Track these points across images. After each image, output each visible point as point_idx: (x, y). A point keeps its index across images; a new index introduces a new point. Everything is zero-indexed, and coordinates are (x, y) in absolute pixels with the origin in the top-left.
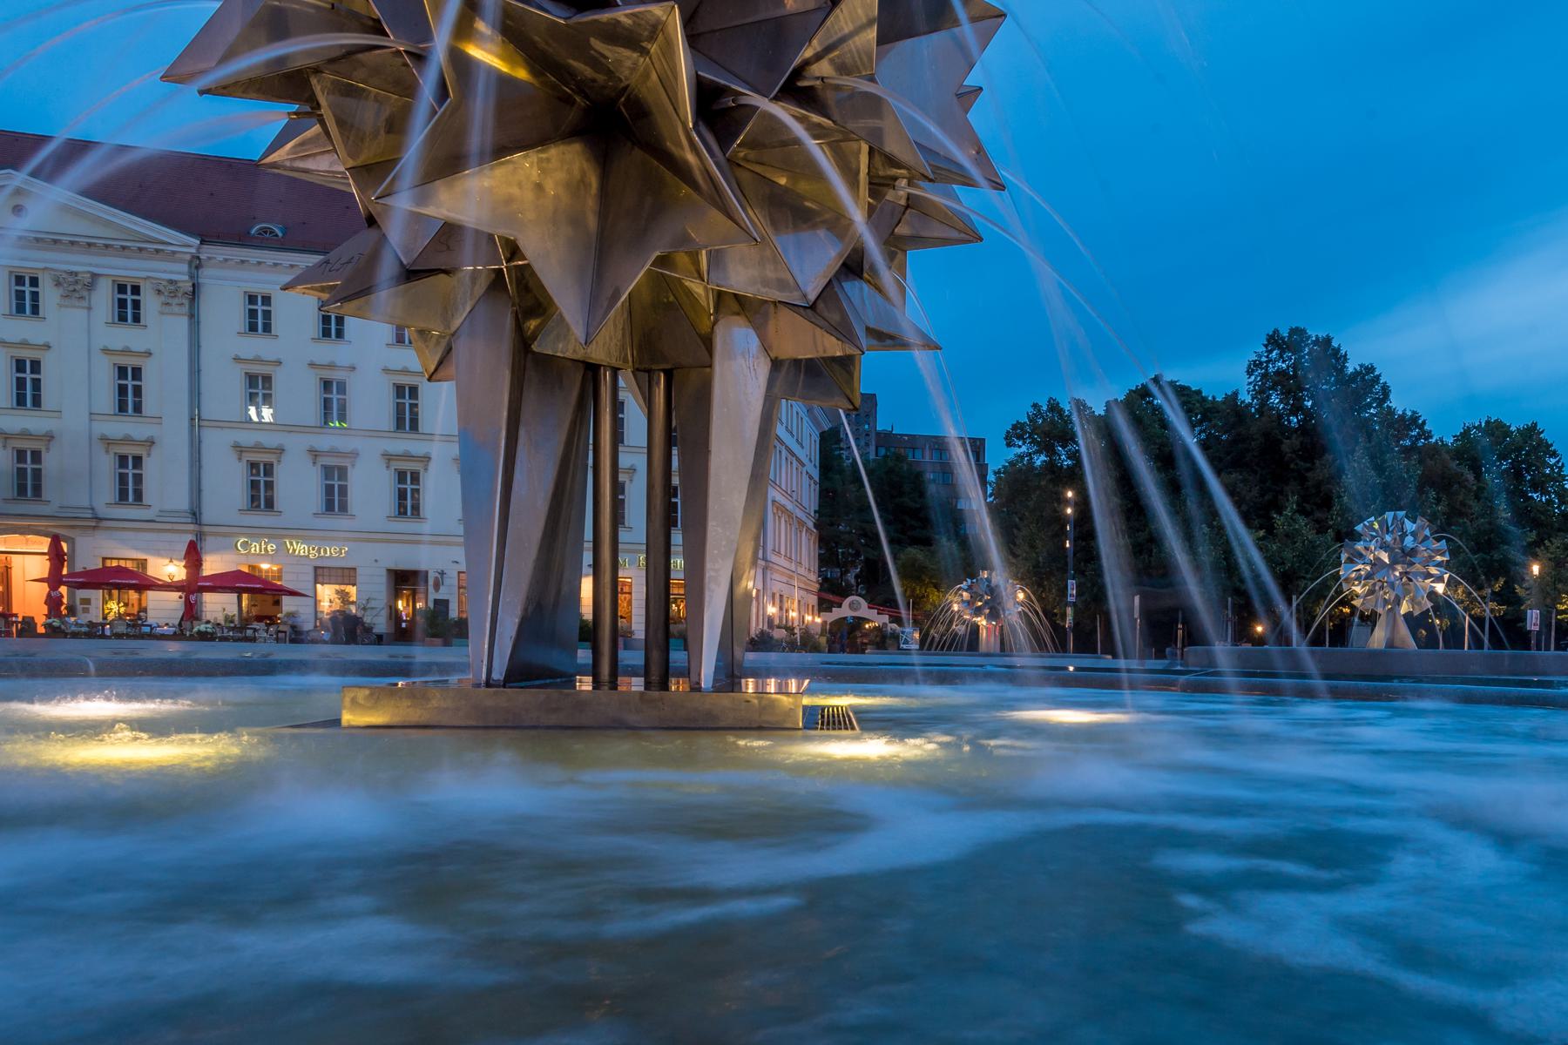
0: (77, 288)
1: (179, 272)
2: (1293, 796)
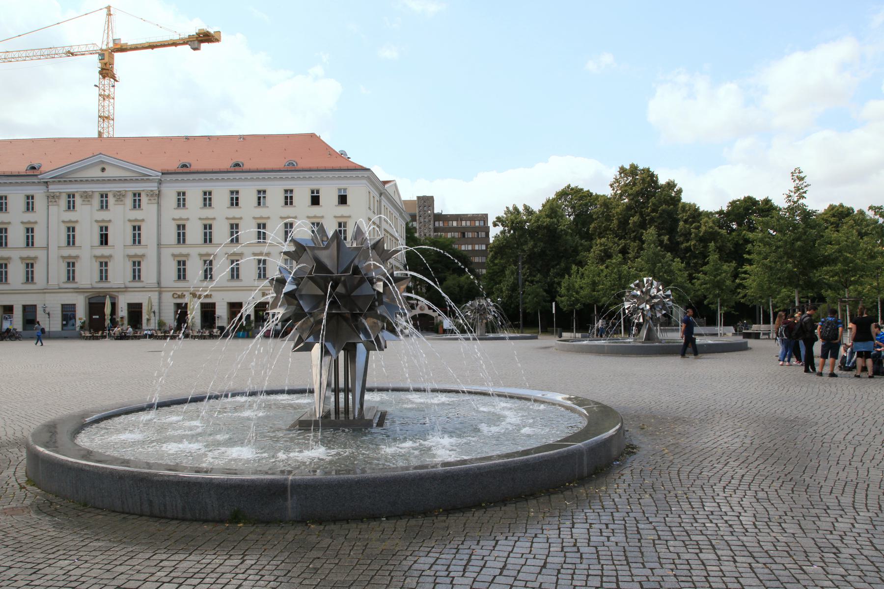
0: (120, 196)
1: (153, 186)
2: (324, 377)
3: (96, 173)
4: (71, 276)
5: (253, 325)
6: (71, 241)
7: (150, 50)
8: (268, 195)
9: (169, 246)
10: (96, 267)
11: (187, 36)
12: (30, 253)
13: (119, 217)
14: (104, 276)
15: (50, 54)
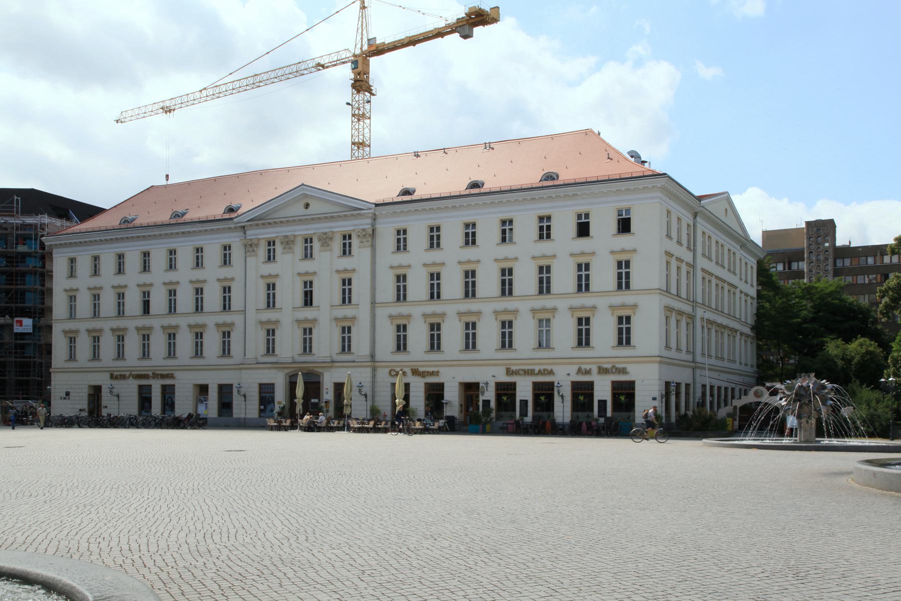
3: (298, 210)
4: (270, 348)
5: (493, 415)
6: (271, 302)
7: (410, 48)
8: (515, 226)
9: (385, 304)
10: (262, 336)
11: (454, 21)
12: (226, 318)
13: (326, 266)
14: (307, 346)
15: (296, 72)
